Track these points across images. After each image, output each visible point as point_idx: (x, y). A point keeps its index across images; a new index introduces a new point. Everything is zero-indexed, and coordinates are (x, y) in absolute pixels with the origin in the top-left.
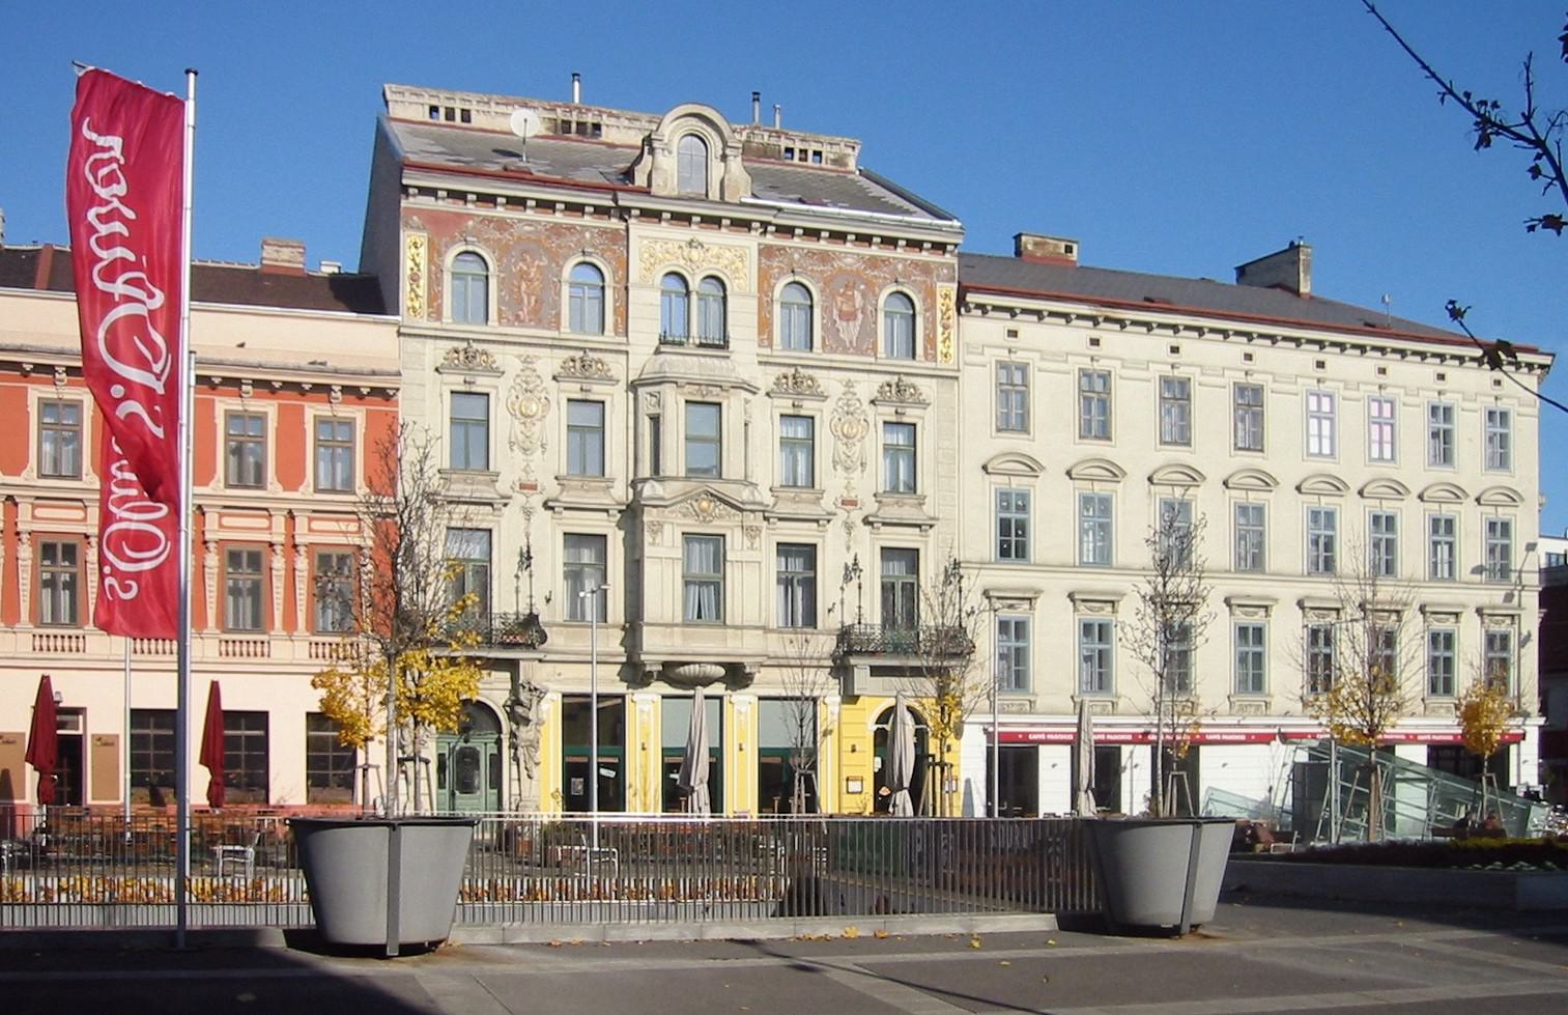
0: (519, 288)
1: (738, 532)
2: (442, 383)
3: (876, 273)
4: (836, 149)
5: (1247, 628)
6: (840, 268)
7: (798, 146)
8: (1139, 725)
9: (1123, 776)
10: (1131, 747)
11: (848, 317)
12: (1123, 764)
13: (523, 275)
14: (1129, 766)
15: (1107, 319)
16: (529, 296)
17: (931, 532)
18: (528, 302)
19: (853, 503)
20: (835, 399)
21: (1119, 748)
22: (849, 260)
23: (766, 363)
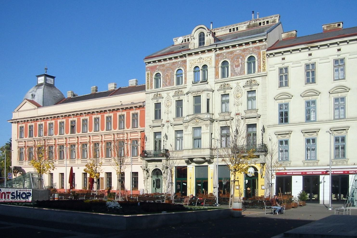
0: (166, 78)
1: (204, 126)
2: (219, 93)
3: (245, 53)
4: (273, 19)
5: (282, 141)
6: (235, 54)
7: (262, 21)
8: (325, 169)
9: (320, 185)
10: (323, 176)
11: (237, 66)
12: (320, 181)
13: (167, 75)
14: (323, 181)
15: (312, 47)
16: (168, 79)
17: (260, 119)
18: (168, 81)
19: (169, 121)
20: (234, 88)
21: (349, 175)
22: (238, 52)
23: (217, 83)
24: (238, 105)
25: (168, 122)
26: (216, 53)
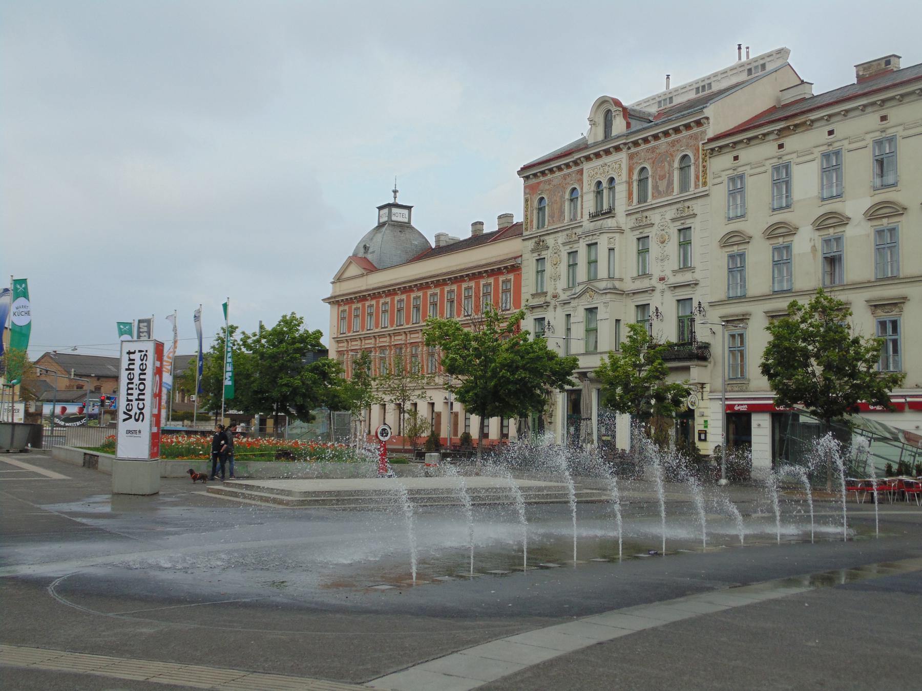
11: (662, 178)
24: (664, 259)
25: (662, 279)
26: (630, 151)
